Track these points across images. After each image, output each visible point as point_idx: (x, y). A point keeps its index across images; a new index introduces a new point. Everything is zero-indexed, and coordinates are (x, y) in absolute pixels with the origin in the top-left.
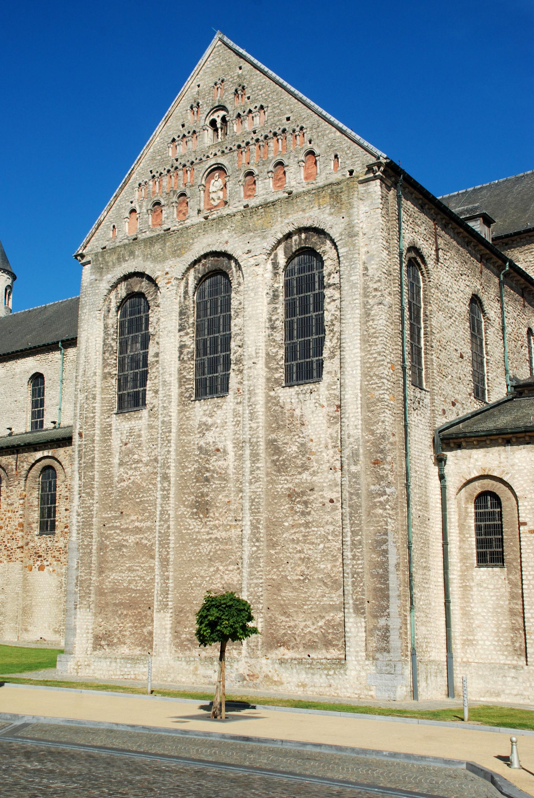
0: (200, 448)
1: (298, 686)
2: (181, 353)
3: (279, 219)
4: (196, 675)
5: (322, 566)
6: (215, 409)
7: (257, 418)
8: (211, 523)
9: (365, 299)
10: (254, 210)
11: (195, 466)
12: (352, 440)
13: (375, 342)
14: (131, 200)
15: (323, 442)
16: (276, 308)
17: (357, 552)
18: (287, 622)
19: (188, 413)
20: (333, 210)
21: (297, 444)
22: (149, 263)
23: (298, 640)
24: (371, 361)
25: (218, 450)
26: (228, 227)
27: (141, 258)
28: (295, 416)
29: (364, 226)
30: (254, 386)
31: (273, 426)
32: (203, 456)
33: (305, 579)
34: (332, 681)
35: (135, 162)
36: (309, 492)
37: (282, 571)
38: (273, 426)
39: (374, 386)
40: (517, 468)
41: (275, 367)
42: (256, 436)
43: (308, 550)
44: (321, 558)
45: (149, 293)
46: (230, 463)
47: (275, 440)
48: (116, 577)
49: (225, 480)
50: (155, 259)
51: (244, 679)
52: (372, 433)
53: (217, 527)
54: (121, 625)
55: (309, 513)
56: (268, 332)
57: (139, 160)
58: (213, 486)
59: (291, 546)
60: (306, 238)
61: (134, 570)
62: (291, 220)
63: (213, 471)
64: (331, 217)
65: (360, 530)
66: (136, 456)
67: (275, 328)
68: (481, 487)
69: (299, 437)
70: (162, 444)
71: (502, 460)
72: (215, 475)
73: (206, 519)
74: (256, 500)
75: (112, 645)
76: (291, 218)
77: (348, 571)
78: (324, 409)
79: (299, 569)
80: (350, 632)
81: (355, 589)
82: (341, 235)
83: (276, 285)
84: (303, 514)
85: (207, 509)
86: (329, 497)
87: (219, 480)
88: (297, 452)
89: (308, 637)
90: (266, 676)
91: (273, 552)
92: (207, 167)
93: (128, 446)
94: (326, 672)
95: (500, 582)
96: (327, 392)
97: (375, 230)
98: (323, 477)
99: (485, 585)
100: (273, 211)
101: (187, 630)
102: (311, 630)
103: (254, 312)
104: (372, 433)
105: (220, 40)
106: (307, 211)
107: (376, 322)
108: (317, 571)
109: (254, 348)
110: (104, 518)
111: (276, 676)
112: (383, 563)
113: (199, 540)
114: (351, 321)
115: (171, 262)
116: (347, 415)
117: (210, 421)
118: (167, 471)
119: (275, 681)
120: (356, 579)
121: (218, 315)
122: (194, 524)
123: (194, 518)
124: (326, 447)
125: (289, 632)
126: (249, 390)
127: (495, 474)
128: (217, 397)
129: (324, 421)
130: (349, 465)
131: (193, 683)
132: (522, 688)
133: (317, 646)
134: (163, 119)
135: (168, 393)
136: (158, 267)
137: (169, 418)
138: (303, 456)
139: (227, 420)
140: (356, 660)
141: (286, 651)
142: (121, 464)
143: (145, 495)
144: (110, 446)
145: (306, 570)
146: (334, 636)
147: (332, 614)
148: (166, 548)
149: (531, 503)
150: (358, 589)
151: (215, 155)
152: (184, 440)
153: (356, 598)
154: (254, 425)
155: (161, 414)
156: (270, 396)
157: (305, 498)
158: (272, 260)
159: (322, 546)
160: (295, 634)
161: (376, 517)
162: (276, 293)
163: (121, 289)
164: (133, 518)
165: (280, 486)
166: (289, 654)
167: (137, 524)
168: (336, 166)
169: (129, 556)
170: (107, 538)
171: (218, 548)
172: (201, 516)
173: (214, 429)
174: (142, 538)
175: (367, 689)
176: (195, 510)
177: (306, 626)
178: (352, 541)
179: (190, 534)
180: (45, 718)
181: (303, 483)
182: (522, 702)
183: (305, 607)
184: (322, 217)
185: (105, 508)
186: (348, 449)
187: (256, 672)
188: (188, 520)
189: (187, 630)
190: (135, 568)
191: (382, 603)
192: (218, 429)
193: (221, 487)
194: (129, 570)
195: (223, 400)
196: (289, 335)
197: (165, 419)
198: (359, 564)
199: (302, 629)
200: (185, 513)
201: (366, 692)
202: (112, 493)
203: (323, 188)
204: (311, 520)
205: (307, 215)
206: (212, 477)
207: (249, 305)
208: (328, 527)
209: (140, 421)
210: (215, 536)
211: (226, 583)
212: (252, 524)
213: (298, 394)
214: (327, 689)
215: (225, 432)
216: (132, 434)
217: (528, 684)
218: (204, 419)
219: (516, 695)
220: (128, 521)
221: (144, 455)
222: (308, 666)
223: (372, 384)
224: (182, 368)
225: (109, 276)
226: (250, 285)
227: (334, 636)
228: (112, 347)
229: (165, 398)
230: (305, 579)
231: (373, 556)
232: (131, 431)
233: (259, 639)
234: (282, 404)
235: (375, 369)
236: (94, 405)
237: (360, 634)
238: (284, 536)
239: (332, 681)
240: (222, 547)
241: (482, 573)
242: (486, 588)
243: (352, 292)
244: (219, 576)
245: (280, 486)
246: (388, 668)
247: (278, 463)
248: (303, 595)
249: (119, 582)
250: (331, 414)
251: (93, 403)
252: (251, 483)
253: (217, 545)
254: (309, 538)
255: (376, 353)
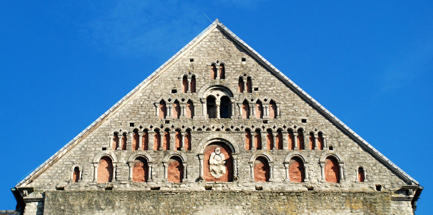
3: (306, 211)
10: (274, 195)
14: (104, 146)
26: (243, 204)
27: (123, 211)
57: (116, 108)
92: (209, 138)
100: (297, 201)
105: (218, 27)
151: (218, 130)
168: (212, 111)
203: (354, 193)
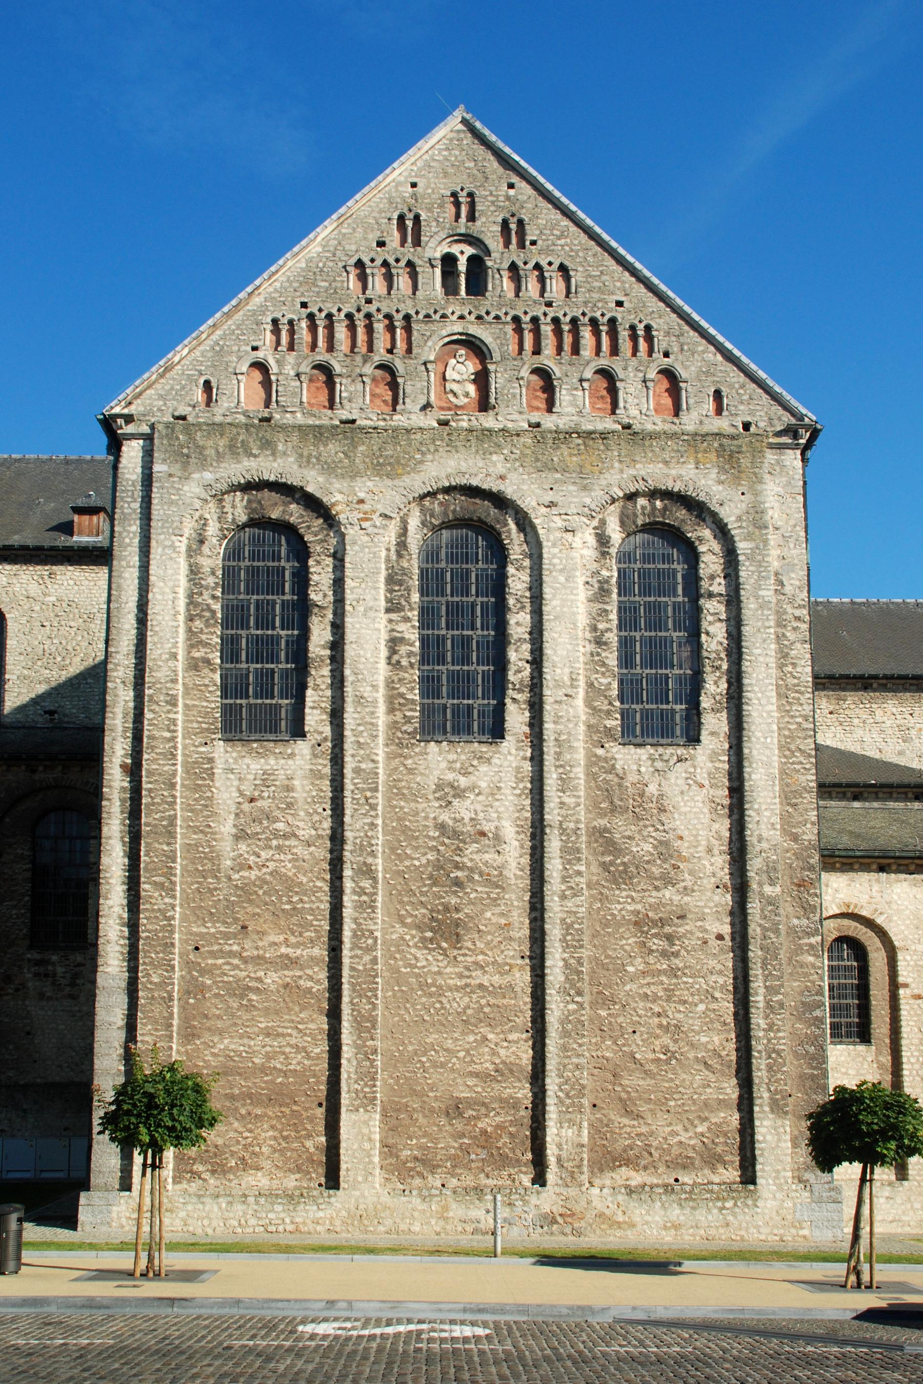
0: (442, 827)
1: (665, 1228)
2: (393, 651)
3: (617, 465)
4: (446, 1219)
5: (704, 1039)
6: (475, 763)
7: (575, 788)
8: (469, 959)
9: (779, 630)
10: (561, 436)
11: (429, 857)
12: (765, 845)
13: (799, 699)
14: (255, 344)
15: (704, 843)
16: (606, 611)
17: (777, 1020)
18: (634, 1126)
19: (410, 761)
20: (723, 477)
21: (651, 840)
22: (313, 473)
23: (656, 1154)
24: (793, 727)
25: (483, 834)
26: (505, 451)
28: (647, 794)
29: (776, 516)
30: (569, 733)
31: (602, 805)
32: (447, 841)
33: (670, 1059)
34: (730, 1218)
35: (265, 275)
36: (676, 921)
37: (624, 1045)
38: (602, 805)
39: (797, 767)
40: (895, 907)
41: (605, 708)
42: (573, 818)
43: (675, 1014)
44: (701, 1027)
45: (309, 527)
46: (510, 860)
47: (606, 830)
48: (232, 1047)
49: (498, 887)
50: (329, 469)
51: (554, 1221)
52: (795, 838)
53: (482, 967)
54: (246, 1134)
55: (676, 955)
56: (590, 647)
58: (472, 896)
59: (641, 1004)
60: (665, 509)
61: (278, 1035)
62: (643, 473)
63: (471, 870)
64: (721, 488)
65: (782, 986)
66: (280, 826)
67: (606, 644)
68: (839, 930)
69: (657, 830)
70: (356, 810)
71: (874, 894)
72: (476, 877)
73: (456, 952)
74: (576, 926)
75: (224, 1172)
76: (642, 469)
77: (760, 1048)
78: (705, 791)
79: (657, 1043)
80: (764, 1141)
81: (772, 1076)
82: (739, 519)
83: (605, 573)
84: (664, 954)
85: (457, 935)
86: (715, 930)
87: (485, 886)
88: (652, 854)
89: (675, 1151)
90: (601, 1215)
91: (603, 1013)
93: (259, 804)
94: (719, 1204)
95: (866, 1066)
96: (710, 765)
97: (795, 526)
98: (704, 898)
99: (843, 1070)
100: (602, 447)
101: (414, 1141)
102: (683, 1140)
103: (565, 609)
104: (795, 838)
106: (672, 465)
107: (799, 669)
108: (692, 1045)
109: (567, 671)
110: (196, 934)
111: (620, 1213)
112: (816, 1037)
113: (440, 987)
114: (761, 659)
115: (370, 484)
116: (756, 806)
117: (463, 782)
118: (370, 860)
119: (619, 1223)
120: (775, 1061)
121: (472, 599)
122: (427, 961)
123: (427, 948)
124: (709, 851)
125: (639, 1143)
126: (556, 740)
127: (864, 913)
128: (479, 742)
129: (706, 810)
130: (760, 884)
131: (438, 1234)
132: (900, 1212)
133: (692, 1164)
134: (334, 217)
135: (368, 719)
136: (337, 486)
137: (371, 765)
138: (665, 861)
139: (502, 785)
140: (775, 1184)
141: (633, 1174)
142: (241, 835)
143: (306, 899)
144: (210, 799)
145: (671, 1044)
146: (726, 1148)
147: (723, 1115)
148: (370, 998)
149: (915, 957)
150: (779, 1076)
151: (462, 317)
152: (402, 808)
153: (776, 1090)
154: (570, 801)
155: (353, 756)
156: (596, 755)
157: (668, 929)
158: (595, 528)
159: (701, 1007)
160: (650, 1146)
161: (802, 967)
162: (606, 586)
163: (233, 507)
164: (272, 938)
165: (619, 907)
166: (637, 1179)
167: (283, 950)
169: (267, 1009)
170: (202, 972)
171: (483, 1002)
172: (444, 945)
173: (472, 797)
174: (300, 977)
175: (795, 1227)
176: (429, 934)
177: (674, 1133)
178: (768, 1002)
179: (418, 976)
180: (666, 1308)
181: (664, 905)
182: (899, 1230)
183: (672, 1103)
184: (703, 482)
185: (197, 913)
186: (760, 860)
187: (577, 1208)
188: (413, 950)
189: (414, 1141)
190: (280, 1030)
191: (814, 1096)
192: (480, 798)
193: (489, 897)
194: (268, 1035)
195: (493, 748)
196: (626, 660)
197: (363, 766)
198: (780, 1038)
199: (665, 1139)
200: (408, 937)
201: (794, 1231)
202: (216, 889)
204: (681, 965)
205: (674, 472)
206: (470, 879)
207: (554, 596)
208: (714, 978)
209: (290, 762)
210: (478, 982)
211: (504, 1062)
212: (567, 965)
213: (653, 760)
214: (721, 1231)
215: (497, 803)
216: (269, 783)
217: (909, 1206)
218: (450, 776)
219: (891, 1222)
220: (260, 944)
221: (301, 824)
222: (683, 1196)
223: (793, 763)
224: (396, 678)
225: (208, 476)
226: (556, 561)
227: (726, 1148)
228: (214, 612)
229: (361, 728)
230: (670, 1059)
231: (798, 1025)
232: (266, 779)
233: (585, 1156)
234: (620, 772)
235: (798, 741)
236: (171, 716)
237: (783, 1145)
238: (628, 988)
239: (730, 1218)
240: (492, 1001)
241: (838, 1053)
242: (846, 1073)
243: (762, 614)
244: (487, 1049)
245: (619, 907)
246: (832, 1193)
247: (612, 869)
248: (667, 1085)
249: (240, 1056)
250: (718, 800)
251: (169, 712)
252: (563, 897)
253: (484, 997)
254: (677, 993)
255: (801, 716)
